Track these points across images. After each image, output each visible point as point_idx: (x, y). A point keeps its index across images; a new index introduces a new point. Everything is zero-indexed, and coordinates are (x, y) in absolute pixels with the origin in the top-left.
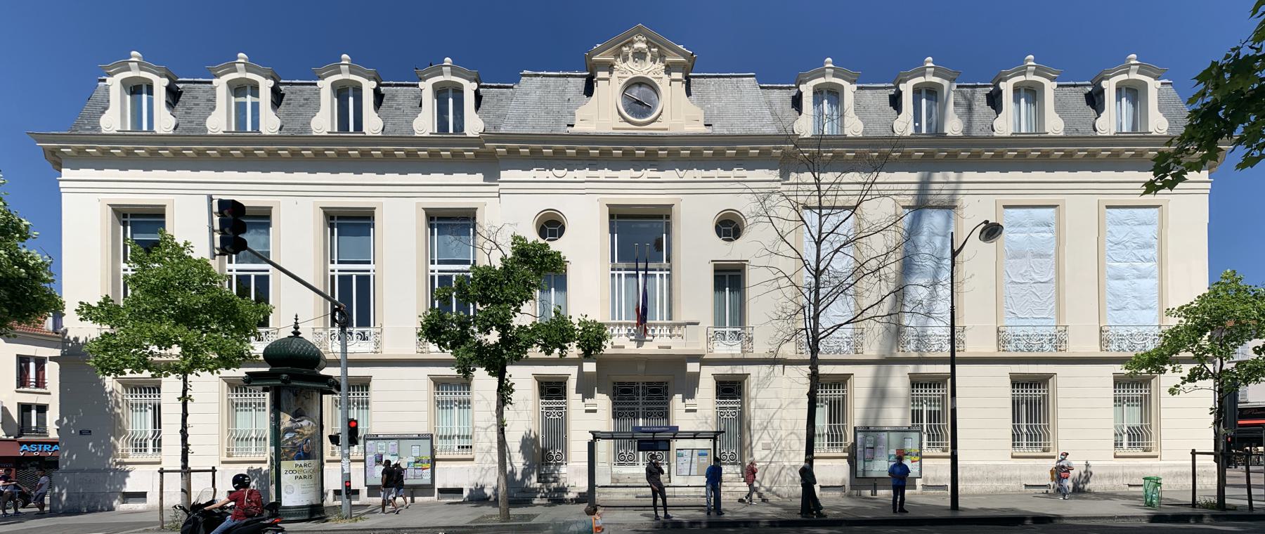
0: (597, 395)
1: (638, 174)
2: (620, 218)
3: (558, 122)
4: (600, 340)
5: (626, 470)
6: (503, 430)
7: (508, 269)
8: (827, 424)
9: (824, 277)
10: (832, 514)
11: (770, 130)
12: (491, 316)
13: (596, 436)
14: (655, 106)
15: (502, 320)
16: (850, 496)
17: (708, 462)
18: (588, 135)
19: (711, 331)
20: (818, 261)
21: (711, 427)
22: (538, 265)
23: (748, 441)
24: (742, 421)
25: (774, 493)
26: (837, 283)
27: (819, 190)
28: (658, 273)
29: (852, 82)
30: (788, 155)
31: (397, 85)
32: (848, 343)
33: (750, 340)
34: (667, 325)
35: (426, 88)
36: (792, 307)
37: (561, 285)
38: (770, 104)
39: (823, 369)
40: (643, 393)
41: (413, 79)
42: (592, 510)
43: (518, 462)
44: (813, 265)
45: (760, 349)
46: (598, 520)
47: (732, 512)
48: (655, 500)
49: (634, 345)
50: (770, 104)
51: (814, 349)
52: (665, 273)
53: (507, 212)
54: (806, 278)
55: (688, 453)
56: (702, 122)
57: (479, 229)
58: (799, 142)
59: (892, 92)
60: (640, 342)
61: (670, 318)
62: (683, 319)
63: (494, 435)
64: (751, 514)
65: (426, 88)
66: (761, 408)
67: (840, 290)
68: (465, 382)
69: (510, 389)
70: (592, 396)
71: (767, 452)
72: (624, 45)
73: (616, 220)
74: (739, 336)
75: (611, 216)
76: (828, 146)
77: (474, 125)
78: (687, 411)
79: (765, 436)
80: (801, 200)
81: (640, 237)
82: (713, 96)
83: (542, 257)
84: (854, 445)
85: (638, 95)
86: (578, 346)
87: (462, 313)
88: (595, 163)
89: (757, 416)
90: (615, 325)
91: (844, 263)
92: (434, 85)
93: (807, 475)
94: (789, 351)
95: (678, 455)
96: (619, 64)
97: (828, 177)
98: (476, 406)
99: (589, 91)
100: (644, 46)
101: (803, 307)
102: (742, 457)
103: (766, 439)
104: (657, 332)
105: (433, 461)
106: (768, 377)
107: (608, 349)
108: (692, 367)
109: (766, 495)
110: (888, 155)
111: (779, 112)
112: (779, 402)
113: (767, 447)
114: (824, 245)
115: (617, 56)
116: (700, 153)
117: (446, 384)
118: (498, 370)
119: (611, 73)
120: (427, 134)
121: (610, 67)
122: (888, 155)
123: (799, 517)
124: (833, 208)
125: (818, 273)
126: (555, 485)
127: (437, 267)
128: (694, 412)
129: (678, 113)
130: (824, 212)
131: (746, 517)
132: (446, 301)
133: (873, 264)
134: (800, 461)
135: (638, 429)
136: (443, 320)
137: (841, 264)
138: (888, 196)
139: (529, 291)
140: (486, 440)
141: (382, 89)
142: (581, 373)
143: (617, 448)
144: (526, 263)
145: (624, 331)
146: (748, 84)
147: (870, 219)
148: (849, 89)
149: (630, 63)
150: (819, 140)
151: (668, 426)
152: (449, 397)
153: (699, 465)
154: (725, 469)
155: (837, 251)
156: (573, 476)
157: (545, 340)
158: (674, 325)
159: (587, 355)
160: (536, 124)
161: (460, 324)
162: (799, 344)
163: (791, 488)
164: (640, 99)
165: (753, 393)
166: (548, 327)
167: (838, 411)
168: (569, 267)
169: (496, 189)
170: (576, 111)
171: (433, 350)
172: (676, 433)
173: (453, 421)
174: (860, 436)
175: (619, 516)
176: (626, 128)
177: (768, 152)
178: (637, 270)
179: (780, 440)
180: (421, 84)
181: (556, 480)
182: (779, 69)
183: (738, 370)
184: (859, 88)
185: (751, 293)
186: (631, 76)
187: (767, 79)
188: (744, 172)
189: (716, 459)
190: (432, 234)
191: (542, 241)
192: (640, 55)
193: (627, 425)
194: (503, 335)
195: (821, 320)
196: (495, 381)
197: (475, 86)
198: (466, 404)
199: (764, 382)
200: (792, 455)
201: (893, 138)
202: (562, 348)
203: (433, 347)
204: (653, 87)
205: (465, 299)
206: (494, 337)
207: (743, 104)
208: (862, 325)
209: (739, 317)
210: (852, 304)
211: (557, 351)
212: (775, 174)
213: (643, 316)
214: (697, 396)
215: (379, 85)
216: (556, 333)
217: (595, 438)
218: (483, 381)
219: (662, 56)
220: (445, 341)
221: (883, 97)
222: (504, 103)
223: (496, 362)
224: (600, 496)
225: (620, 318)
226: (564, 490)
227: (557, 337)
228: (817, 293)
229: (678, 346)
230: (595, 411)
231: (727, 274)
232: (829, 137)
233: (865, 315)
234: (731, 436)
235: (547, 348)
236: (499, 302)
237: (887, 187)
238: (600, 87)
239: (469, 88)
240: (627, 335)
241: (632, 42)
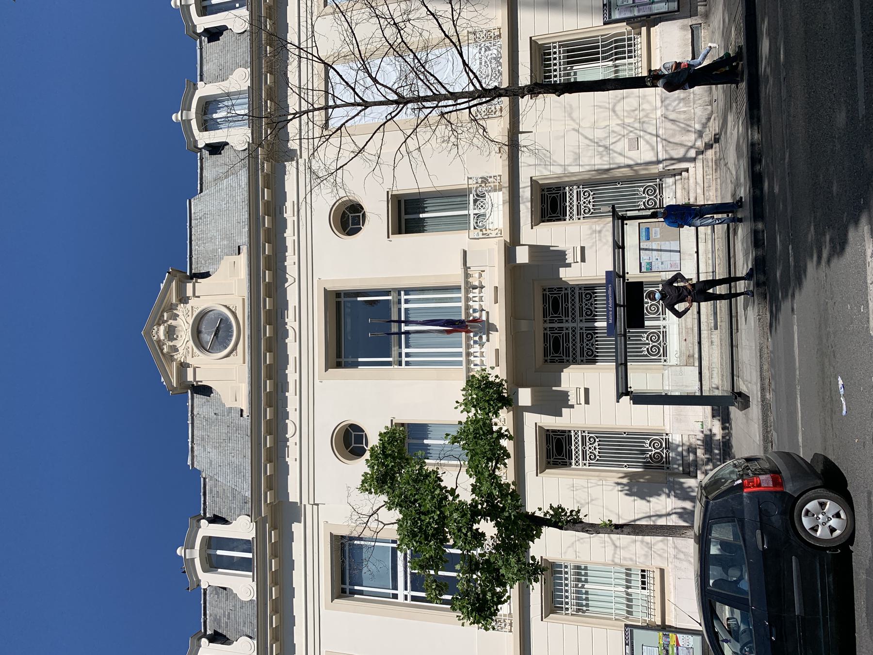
0: (564, 386)
1: (291, 333)
2: (342, 353)
3: (238, 428)
4: (490, 384)
5: (674, 344)
6: (617, 527)
7: (400, 502)
8: (600, 64)
9: (406, 93)
10: (737, 39)
11: (243, 177)
12: (460, 530)
13: (623, 390)
14: (221, 314)
15: (463, 515)
16: (706, 16)
17: (658, 227)
18: (251, 392)
19: (474, 233)
20: (388, 102)
21: (607, 225)
22: (396, 462)
23: (627, 172)
24: (597, 183)
25: (705, 126)
26: (412, 75)
27: (307, 112)
28: (404, 306)
29: (195, 88)
30: (271, 153)
31: (205, 614)
32: (488, 49)
33: (485, 180)
34: (467, 292)
35: (208, 579)
36: (443, 130)
37: (419, 431)
38: (217, 179)
39: (525, 79)
40: (558, 322)
41: (197, 593)
42: (742, 400)
43: (664, 505)
44: (391, 108)
45: (496, 166)
46: (749, 384)
47: (737, 185)
48: (721, 297)
49: (494, 336)
50: (217, 179)
51: (495, 93)
52: (403, 297)
53: (336, 498)
54: (407, 115)
55: (645, 255)
56: (235, 258)
57: (355, 534)
58: (256, 142)
59: (205, 39)
60: (489, 328)
61: (457, 289)
62: (460, 271)
63: (623, 539)
64: (739, 156)
65: (208, 579)
66: (578, 157)
67: (421, 69)
68: (548, 571)
69: (558, 511)
70: (565, 394)
71: (642, 142)
72: (162, 350)
73: (343, 360)
74: (480, 196)
75: (339, 365)
76: (260, 107)
77: (242, 528)
78: (583, 260)
79: (618, 147)
80: (318, 132)
81: (363, 328)
82: (210, 246)
83: (386, 456)
84: (628, 21)
85: (209, 334)
86: (496, 414)
87: (458, 567)
88: (281, 386)
89: (591, 162)
90: (468, 362)
91: (389, 68)
92: (205, 571)
93: (679, 78)
94: (498, 127)
95: (650, 270)
96: (179, 356)
97: (293, 103)
98: (583, 559)
99: (206, 391)
100: (162, 328)
101: (442, 115)
102: (651, 178)
103: (622, 145)
104: (476, 306)
105: (664, 628)
106: (534, 153)
107: (499, 373)
108: (522, 256)
109: (708, 137)
110: (270, 34)
111: (226, 168)
112: (567, 134)
113: (635, 144)
114: (368, 98)
115: (171, 359)
116: (268, 258)
117: (553, 596)
118: (533, 525)
119: (188, 366)
120: (254, 585)
121: (183, 366)
122: (270, 34)
123: (743, 85)
124: (326, 92)
125: (402, 101)
126: (700, 452)
127: (401, 592)
128: (585, 250)
129: (226, 287)
130: (331, 103)
131: (744, 163)
132: (443, 585)
133: (390, 32)
134: (654, 94)
135: (611, 329)
136: (466, 594)
137: (390, 72)
138: (313, 26)
139: (427, 475)
140: (633, 549)
141: (209, 632)
142: (537, 408)
143: (642, 358)
144: (393, 478)
145: (476, 349)
146: (198, 206)
147: (338, 43)
148: (204, 90)
149: (178, 343)
150: (254, 119)
151: (606, 285)
152: (571, 595)
153: (664, 238)
154: (669, 200)
155: (375, 80)
156: (687, 426)
157: (490, 460)
158: (467, 283)
159: (509, 402)
160: (240, 453)
161: (473, 572)
162: (489, 115)
163: (697, 101)
164: (213, 332)
165: (557, 170)
166: (473, 454)
167: (582, 51)
168: (400, 419)
169: (309, 508)
170: (227, 406)
171: (508, 610)
172: (616, 275)
173: (605, 591)
174: (616, 15)
175: (748, 354)
176: (244, 347)
177: (267, 177)
178: (400, 333)
179: (623, 125)
180: (204, 585)
181: (692, 450)
182: (179, 172)
183: (525, 193)
184: (201, 80)
185: (425, 185)
186: (191, 343)
187: (192, 186)
188: (289, 204)
189: (654, 215)
190: (361, 593)
191: (367, 455)
192: (171, 333)
193: (605, 343)
194: (484, 514)
195: (458, 89)
196: (548, 532)
197: (204, 522)
198: (580, 572)
199: (542, 156)
200: (646, 106)
201: (251, 32)
202: (501, 435)
203: (504, 609)
204: (202, 317)
205: (441, 560)
206: (488, 528)
207: (219, 210)
208: (463, 34)
209: (455, 197)
210: (437, 52)
211: (504, 442)
212: (290, 167)
213: (456, 326)
214: (561, 247)
215: (205, 635)
216: (481, 444)
217: (627, 393)
218: (548, 546)
219: (172, 308)
220: (494, 594)
221: (211, 49)
222: (220, 490)
223: (522, 527)
224: (716, 383)
225: (459, 354)
226: (708, 441)
227: (483, 445)
228: (426, 99)
229: (493, 276)
230: (587, 391)
231: (404, 217)
232: (251, 108)
233: (451, 32)
234: (621, 196)
235: (500, 456)
236: (443, 520)
237: (303, 29)
238: (203, 378)
239: (207, 529)
240: (482, 345)
241: (159, 341)
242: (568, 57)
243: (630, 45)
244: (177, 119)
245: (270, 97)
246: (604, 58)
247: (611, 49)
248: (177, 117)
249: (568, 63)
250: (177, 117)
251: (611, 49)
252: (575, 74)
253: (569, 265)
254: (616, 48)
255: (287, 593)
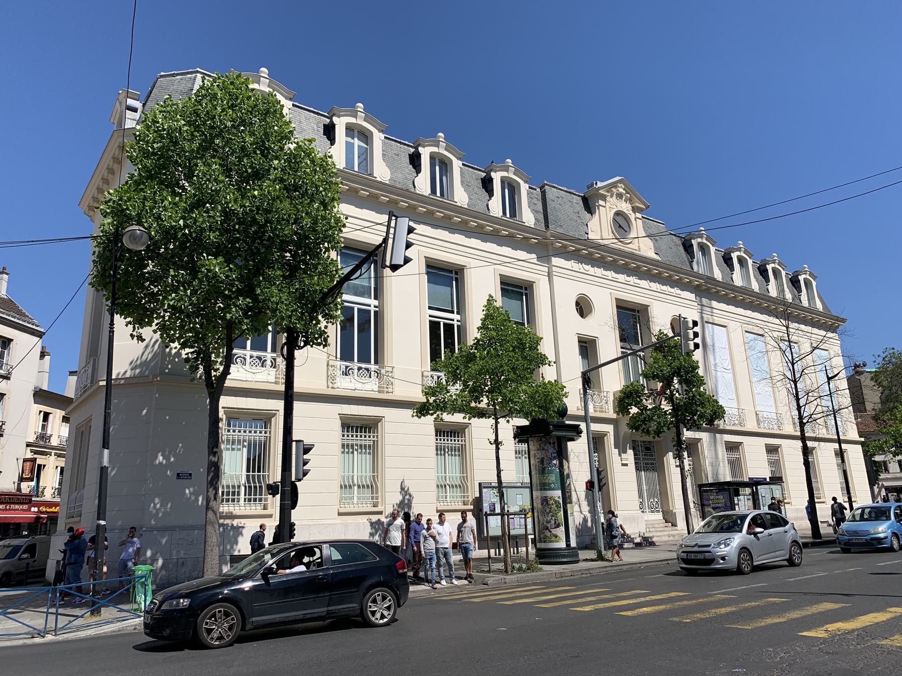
51: (802, 431)
219: (630, 200)
231: (356, 307)
242: (255, 445)
243: (255, 500)
244: (262, 72)
245: (351, 190)
246: (248, 477)
247: (254, 482)
248: (265, 73)
249: (250, 445)
250: (265, 73)
251: (254, 482)
252: (239, 450)
253: (620, 455)
254: (255, 487)
255: (453, 228)
